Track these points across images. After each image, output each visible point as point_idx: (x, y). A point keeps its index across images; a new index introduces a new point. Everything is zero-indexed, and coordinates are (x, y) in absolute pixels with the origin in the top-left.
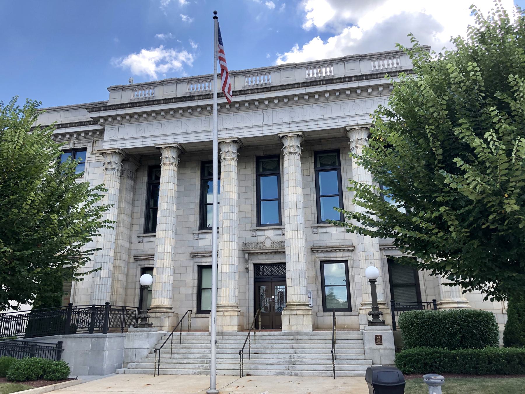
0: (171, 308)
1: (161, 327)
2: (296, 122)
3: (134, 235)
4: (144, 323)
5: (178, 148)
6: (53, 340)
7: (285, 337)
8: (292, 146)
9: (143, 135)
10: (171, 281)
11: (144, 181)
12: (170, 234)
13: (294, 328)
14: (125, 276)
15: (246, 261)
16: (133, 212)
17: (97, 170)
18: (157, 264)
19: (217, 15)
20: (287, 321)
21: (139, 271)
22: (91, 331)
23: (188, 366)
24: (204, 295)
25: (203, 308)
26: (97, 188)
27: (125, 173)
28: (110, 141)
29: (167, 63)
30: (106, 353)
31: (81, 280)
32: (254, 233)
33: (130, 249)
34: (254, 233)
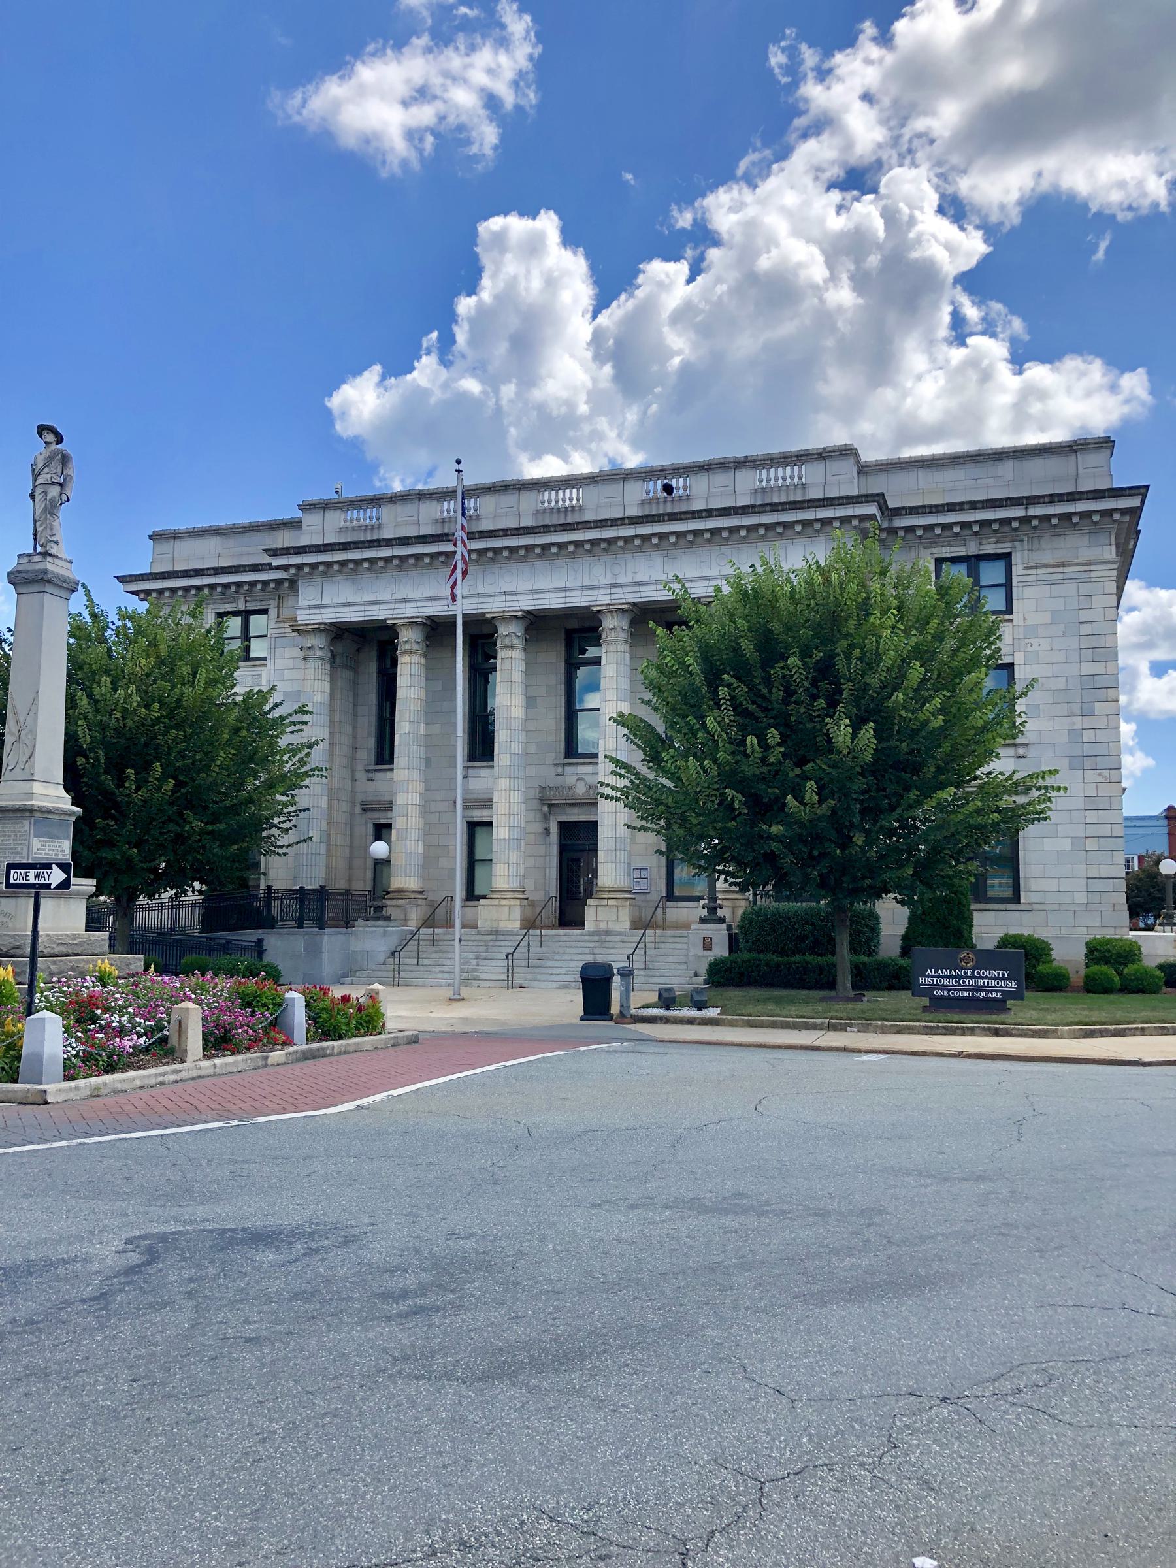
0: (421, 893)
1: (405, 922)
2: (622, 585)
3: (360, 767)
4: (378, 914)
5: (425, 624)
6: (250, 936)
7: (587, 938)
9: (366, 598)
11: (371, 669)
12: (415, 775)
13: (603, 925)
14: (348, 838)
15: (546, 818)
16: (354, 727)
18: (398, 823)
19: (461, 467)
20: (592, 912)
21: (370, 830)
22: (300, 926)
23: (440, 975)
24: (479, 871)
26: (296, 712)
27: (338, 661)
28: (310, 608)
29: (435, 97)
30: (325, 955)
31: (285, 854)
32: (560, 770)
33: (353, 792)
34: (560, 770)
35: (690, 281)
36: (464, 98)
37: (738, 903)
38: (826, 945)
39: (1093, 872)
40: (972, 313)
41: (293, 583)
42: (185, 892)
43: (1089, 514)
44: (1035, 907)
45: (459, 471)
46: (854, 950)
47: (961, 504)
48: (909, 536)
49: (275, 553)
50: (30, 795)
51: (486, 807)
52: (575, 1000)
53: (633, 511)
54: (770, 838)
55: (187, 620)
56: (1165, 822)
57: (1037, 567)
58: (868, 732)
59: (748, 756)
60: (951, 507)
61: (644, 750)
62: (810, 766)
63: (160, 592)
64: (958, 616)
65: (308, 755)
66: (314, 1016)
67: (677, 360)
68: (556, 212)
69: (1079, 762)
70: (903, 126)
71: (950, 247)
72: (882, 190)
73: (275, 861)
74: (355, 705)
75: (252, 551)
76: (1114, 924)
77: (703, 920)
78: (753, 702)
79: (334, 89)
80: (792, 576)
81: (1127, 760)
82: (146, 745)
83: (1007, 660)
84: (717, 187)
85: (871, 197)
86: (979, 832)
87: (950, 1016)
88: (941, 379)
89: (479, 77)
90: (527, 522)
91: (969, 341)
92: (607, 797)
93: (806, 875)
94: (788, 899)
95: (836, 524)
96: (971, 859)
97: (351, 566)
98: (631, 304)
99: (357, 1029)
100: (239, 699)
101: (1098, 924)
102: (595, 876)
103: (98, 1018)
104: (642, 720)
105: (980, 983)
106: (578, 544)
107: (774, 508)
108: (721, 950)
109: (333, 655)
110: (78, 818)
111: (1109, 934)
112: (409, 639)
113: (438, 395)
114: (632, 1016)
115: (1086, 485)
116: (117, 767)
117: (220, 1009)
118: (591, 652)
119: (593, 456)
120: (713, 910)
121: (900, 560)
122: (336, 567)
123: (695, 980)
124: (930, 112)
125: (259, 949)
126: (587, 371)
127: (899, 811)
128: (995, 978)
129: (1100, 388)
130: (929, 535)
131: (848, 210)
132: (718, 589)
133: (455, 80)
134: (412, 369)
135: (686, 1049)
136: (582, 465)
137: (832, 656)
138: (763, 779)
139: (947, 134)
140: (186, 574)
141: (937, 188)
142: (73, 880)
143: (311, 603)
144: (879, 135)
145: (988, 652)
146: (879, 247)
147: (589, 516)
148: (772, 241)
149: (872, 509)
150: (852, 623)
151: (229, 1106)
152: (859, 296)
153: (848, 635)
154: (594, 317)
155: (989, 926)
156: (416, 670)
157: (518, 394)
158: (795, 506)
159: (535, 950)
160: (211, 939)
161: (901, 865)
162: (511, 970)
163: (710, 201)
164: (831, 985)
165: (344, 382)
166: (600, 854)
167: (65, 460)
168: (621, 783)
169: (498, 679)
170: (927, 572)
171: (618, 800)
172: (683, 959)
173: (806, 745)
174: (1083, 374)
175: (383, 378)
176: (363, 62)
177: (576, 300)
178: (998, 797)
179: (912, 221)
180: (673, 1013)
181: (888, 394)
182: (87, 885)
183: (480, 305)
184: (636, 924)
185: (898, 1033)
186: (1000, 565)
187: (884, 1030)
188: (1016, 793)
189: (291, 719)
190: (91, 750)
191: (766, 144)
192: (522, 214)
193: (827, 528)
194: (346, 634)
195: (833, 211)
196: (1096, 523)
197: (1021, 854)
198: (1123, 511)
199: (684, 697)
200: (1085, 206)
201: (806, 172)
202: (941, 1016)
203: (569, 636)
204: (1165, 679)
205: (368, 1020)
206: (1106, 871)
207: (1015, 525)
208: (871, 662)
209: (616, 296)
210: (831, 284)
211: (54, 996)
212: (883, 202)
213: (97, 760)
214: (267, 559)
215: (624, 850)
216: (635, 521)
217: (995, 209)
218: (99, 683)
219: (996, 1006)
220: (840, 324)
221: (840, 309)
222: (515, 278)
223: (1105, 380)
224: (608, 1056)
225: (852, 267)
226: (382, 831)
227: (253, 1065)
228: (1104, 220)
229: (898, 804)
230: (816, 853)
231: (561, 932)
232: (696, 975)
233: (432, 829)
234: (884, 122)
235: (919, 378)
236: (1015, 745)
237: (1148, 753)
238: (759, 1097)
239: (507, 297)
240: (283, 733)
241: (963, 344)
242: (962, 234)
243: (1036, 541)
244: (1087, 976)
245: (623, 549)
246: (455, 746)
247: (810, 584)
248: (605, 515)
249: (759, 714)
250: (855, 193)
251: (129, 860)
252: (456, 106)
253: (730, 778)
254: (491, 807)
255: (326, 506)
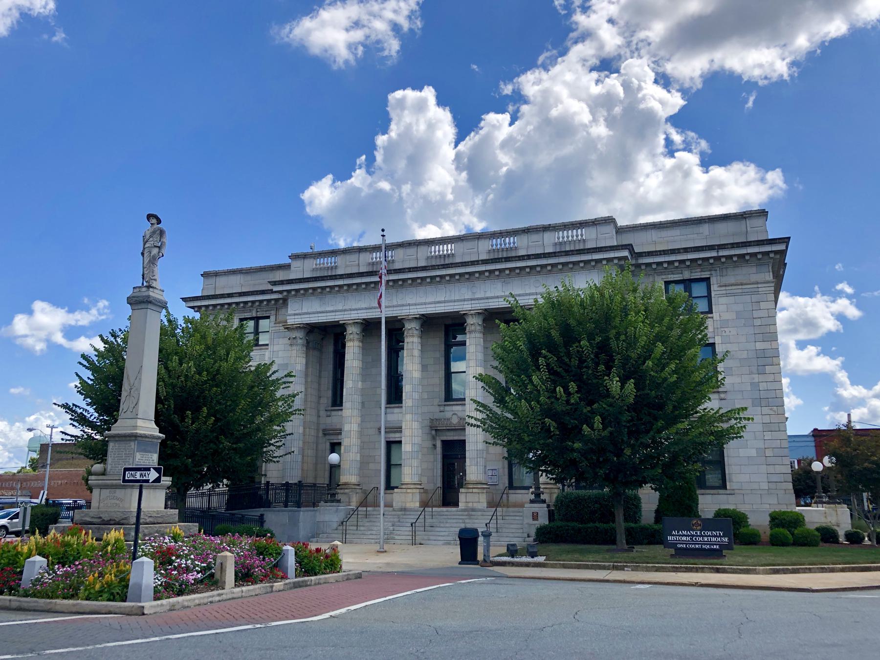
1: (349, 503)
3: (322, 408)
6: (256, 512)
8: (473, 323)
10: (358, 459)
11: (330, 349)
12: (356, 412)
13: (470, 505)
15: (434, 438)
16: (319, 384)
17: (281, 341)
18: (345, 442)
19: (384, 233)
20: (464, 497)
21: (328, 446)
22: (286, 506)
23: (371, 537)
24: (394, 471)
25: (392, 485)
27: (311, 345)
28: (295, 315)
29: (364, 26)
30: (301, 524)
32: (442, 408)
33: (318, 424)
34: (442, 408)
35: (511, 124)
36: (380, 26)
37: (553, 491)
38: (609, 517)
39: (771, 469)
40: (677, 138)
41: (285, 301)
42: (218, 486)
43: (755, 254)
44: (736, 491)
45: (383, 236)
46: (626, 520)
47: (678, 249)
48: (648, 269)
49: (274, 283)
50: (135, 427)
51: (397, 432)
52: (455, 552)
53: (484, 257)
54: (573, 450)
55: (225, 323)
56: (813, 439)
57: (726, 286)
58: (630, 385)
59: (558, 399)
60: (673, 252)
61: (494, 396)
62: (595, 406)
63: (207, 307)
64: (680, 315)
65: (293, 401)
66: (299, 561)
67: (504, 169)
68: (433, 87)
69: (759, 402)
70: (632, 36)
71: (662, 102)
72: (622, 71)
73: (271, 466)
74: (320, 372)
75: (261, 282)
76: (787, 503)
77: (532, 502)
78: (560, 367)
79: (307, 23)
80: (580, 293)
81: (786, 400)
82: (198, 397)
83: (711, 341)
84: (526, 71)
85: (615, 75)
86: (701, 447)
87: (687, 560)
88: (660, 176)
89: (389, 15)
90: (422, 263)
91: (676, 154)
92: (472, 425)
93: (596, 474)
94: (585, 488)
95: (604, 262)
96: (696, 462)
97: (319, 290)
98: (477, 138)
99: (325, 569)
100: (253, 369)
101: (776, 502)
102: (465, 474)
103: (173, 561)
104: (493, 378)
105: (706, 539)
106: (452, 276)
107: (567, 253)
108: (544, 520)
109: (308, 342)
110: (163, 441)
111: (784, 508)
112: (352, 332)
113: (366, 191)
114: (491, 562)
115: (752, 238)
116: (180, 410)
117: (245, 557)
118: (460, 338)
119: (455, 224)
120: (538, 495)
121: (644, 282)
122: (310, 291)
123: (527, 539)
124: (648, 28)
125: (261, 520)
126: (451, 175)
127: (652, 433)
128: (715, 536)
129: (754, 181)
130: (660, 268)
131: (602, 82)
132: (536, 301)
133: (375, 16)
134: (350, 177)
135: (526, 582)
136: (450, 230)
137: (608, 339)
138: (567, 413)
139: (658, 40)
140: (222, 296)
141: (653, 70)
142: (163, 478)
143: (297, 312)
144: (619, 41)
145: (700, 336)
146: (621, 102)
147: (458, 260)
148: (558, 101)
149: (626, 253)
150: (618, 320)
151: (253, 616)
152: (610, 130)
153: (615, 327)
154: (456, 146)
155: (708, 504)
156: (357, 350)
157: (412, 190)
158: (508, 259)
159: (429, 521)
160: (233, 514)
161: (653, 467)
162: (414, 534)
163: (523, 79)
164: (613, 542)
165: (311, 185)
166: (467, 460)
167: (162, 233)
168: (480, 416)
169: (405, 355)
170: (661, 289)
171: (478, 426)
172: (519, 526)
173: (593, 392)
174: (744, 173)
175: (334, 182)
176: (324, 9)
177: (445, 135)
178: (711, 424)
179: (640, 88)
180: (516, 560)
181: (629, 185)
182: (167, 481)
183: (390, 140)
184: (491, 504)
185: (656, 571)
186: (703, 285)
187: (648, 570)
188: (722, 422)
189: (283, 380)
190: (166, 400)
191: (555, 47)
192: (413, 89)
193: (599, 265)
194: (316, 330)
195: (593, 84)
196: (760, 259)
197: (726, 459)
198: (776, 252)
199: (518, 364)
200: (740, 77)
201: (578, 62)
202: (682, 560)
203: (447, 329)
204: (806, 351)
205: (332, 564)
206: (779, 469)
207: (711, 261)
208: (632, 342)
209: (468, 134)
210: (594, 124)
211: (147, 548)
212: (624, 77)
213: (169, 406)
214: (270, 287)
215: (482, 456)
216: (485, 262)
217: (688, 80)
218: (171, 361)
219: (715, 554)
220: (599, 146)
221: (599, 138)
222: (410, 124)
223: (758, 176)
224: (476, 585)
225: (605, 114)
226: (335, 447)
227: (264, 591)
228: (751, 85)
229: (651, 429)
230: (601, 459)
231: (445, 509)
232: (529, 536)
233: (365, 445)
234: (621, 34)
235: (648, 176)
236: (718, 392)
237: (798, 396)
238: (575, 611)
239: (406, 135)
240: (278, 388)
241: (673, 156)
242: (668, 95)
243: (724, 270)
244: (771, 535)
245: (478, 278)
246: (380, 395)
247: (592, 297)
248: (407, 265)
249: (564, 374)
250: (606, 72)
251: (186, 466)
252: (376, 30)
253: (548, 412)
254: (401, 432)
255: (305, 256)
